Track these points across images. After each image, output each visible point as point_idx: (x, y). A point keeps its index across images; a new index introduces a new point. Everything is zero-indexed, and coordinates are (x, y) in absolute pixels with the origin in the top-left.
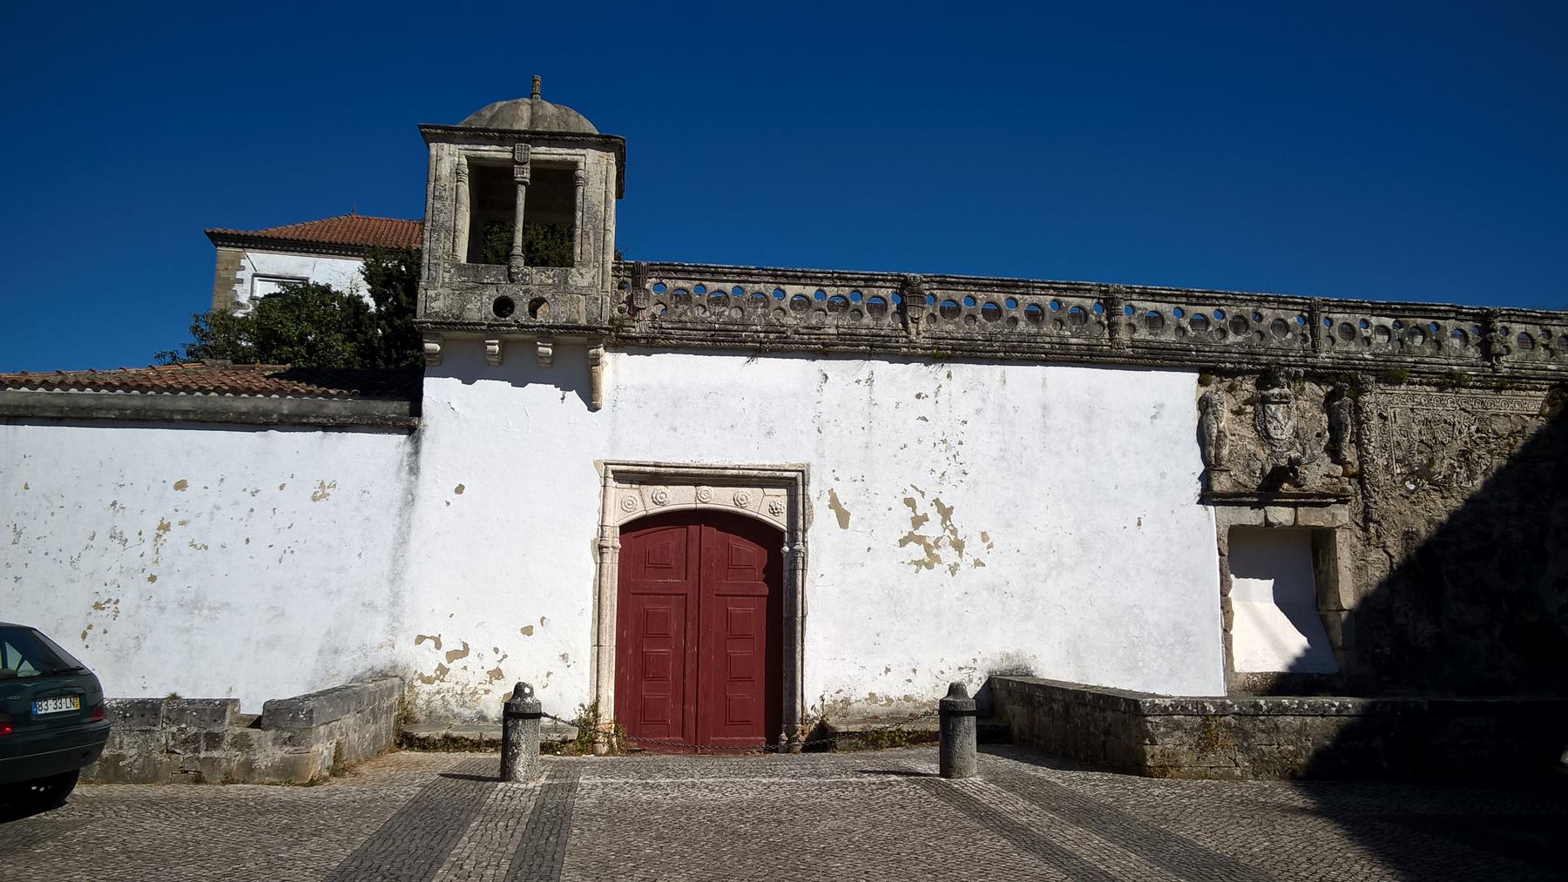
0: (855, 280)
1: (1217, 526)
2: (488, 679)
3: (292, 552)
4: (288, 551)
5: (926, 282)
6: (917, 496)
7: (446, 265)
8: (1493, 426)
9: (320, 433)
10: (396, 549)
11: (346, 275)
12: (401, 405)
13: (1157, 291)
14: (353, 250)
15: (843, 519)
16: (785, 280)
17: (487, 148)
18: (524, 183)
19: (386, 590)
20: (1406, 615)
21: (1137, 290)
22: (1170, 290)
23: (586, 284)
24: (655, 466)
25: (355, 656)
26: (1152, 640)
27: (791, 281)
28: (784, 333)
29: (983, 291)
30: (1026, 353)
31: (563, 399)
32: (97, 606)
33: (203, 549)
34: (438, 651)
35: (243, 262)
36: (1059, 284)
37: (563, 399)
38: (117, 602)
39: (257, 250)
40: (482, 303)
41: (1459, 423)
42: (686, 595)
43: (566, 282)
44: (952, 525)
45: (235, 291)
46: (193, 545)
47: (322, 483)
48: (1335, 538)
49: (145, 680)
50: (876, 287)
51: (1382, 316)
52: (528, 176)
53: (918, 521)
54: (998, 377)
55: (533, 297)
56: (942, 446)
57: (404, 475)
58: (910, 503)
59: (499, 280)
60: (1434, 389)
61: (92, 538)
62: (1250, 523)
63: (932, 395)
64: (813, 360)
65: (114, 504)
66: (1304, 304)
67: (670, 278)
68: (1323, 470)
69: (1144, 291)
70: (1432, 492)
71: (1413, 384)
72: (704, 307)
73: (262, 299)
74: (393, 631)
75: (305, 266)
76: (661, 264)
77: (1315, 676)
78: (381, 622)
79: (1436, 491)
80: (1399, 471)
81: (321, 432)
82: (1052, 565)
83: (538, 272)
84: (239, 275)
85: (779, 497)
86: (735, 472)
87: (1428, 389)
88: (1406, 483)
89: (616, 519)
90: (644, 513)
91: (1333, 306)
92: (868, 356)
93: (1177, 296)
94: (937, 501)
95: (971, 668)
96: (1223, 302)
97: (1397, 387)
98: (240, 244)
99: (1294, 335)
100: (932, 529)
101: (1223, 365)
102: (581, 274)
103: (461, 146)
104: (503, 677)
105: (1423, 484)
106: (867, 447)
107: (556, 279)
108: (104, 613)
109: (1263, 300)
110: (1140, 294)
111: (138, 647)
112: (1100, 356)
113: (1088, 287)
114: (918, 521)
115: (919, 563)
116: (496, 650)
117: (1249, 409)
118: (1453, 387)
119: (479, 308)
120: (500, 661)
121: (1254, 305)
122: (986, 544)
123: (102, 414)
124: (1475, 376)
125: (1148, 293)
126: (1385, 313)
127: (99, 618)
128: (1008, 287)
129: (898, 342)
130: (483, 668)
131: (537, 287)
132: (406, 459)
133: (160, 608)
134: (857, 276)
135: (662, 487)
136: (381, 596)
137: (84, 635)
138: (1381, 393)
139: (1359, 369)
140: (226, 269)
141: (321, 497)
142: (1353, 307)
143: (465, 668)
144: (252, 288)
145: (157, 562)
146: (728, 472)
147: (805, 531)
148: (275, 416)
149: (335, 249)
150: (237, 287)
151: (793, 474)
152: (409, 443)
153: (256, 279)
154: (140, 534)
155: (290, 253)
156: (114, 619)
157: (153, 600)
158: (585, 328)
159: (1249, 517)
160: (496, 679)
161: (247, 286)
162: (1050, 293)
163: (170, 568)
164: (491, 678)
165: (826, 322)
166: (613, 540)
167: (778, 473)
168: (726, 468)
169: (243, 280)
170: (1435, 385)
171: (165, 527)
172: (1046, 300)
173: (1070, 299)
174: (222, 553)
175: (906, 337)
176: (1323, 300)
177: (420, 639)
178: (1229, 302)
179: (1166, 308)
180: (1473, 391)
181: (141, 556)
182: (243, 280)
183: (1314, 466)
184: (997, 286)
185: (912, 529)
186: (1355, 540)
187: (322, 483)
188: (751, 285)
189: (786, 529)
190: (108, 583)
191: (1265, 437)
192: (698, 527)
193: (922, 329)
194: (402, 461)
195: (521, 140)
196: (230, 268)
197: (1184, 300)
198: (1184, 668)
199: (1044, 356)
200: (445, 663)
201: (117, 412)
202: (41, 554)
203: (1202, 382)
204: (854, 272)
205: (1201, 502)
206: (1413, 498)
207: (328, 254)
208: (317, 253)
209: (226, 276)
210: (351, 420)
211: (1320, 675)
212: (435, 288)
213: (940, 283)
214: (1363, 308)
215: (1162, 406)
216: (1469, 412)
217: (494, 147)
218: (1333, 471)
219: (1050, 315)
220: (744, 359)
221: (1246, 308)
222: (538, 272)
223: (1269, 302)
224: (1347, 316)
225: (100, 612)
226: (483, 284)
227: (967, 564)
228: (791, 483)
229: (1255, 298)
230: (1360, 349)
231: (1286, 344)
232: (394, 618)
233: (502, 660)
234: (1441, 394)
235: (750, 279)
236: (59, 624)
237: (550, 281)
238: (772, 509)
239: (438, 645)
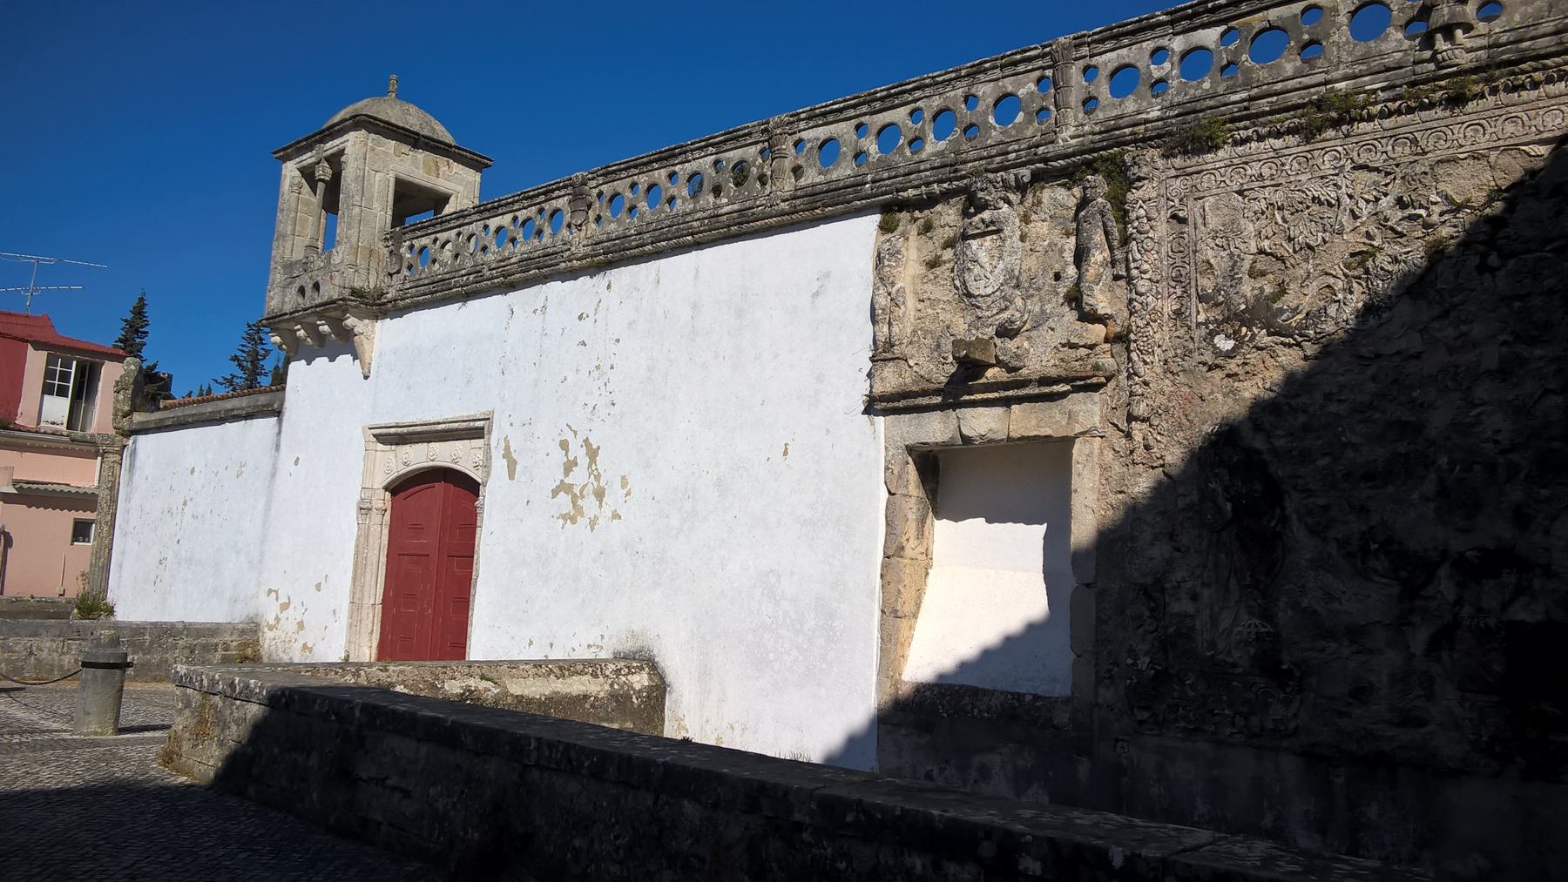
1: (886, 448)
5: (593, 179)
6: (569, 436)
8: (1441, 187)
13: (827, 109)
18: (322, 180)
20: (1194, 597)
21: (802, 116)
22: (845, 101)
26: (789, 622)
27: (492, 214)
28: (480, 272)
29: (643, 173)
30: (671, 239)
36: (717, 137)
41: (1350, 197)
44: (596, 469)
48: (1071, 455)
50: (554, 199)
51: (1195, 29)
53: (569, 466)
54: (652, 278)
56: (596, 374)
57: (273, 452)
58: (564, 445)
60: (1291, 140)
62: (933, 440)
63: (591, 315)
66: (1043, 56)
67: (417, 238)
68: (1059, 337)
69: (812, 113)
70: (1280, 350)
71: (1244, 141)
77: (1029, 698)
79: (1289, 346)
80: (1202, 318)
82: (685, 515)
87: (1278, 143)
88: (1216, 341)
89: (381, 479)
91: (1094, 42)
93: (854, 107)
94: (586, 441)
95: (598, 647)
96: (918, 94)
97: (1209, 157)
99: (1027, 114)
100: (579, 477)
101: (905, 194)
105: (1254, 336)
109: (976, 72)
110: (809, 118)
112: (748, 223)
113: (746, 131)
114: (569, 466)
115: (564, 517)
117: (948, 254)
118: (1336, 124)
121: (965, 83)
122: (625, 491)
124: (1383, 89)
125: (817, 116)
126: (1197, 21)
128: (666, 159)
129: (562, 257)
138: (1177, 177)
139: (1127, 143)
142: (1133, 33)
146: (440, 427)
159: (935, 428)
162: (709, 152)
165: (516, 251)
166: (383, 500)
167: (472, 424)
168: (439, 423)
170: (1291, 131)
172: (705, 163)
173: (731, 154)
176: (1075, 39)
177: (270, 591)
178: (928, 92)
179: (843, 130)
180: (1387, 123)
183: (1043, 330)
184: (656, 161)
185: (562, 477)
186: (1109, 455)
188: (467, 227)
191: (964, 294)
193: (579, 241)
197: (865, 109)
198: (824, 666)
199: (689, 238)
203: (886, 228)
204: (536, 187)
205: (867, 411)
206: (1232, 366)
211: (1036, 697)
213: (604, 175)
214: (1152, 27)
215: (828, 275)
216: (1377, 170)
218: (1081, 336)
219: (709, 182)
221: (952, 93)
223: (985, 71)
224: (1125, 51)
227: (605, 517)
229: (963, 72)
230: (1145, 104)
231: (1014, 132)
234: (1308, 147)
235: (466, 221)
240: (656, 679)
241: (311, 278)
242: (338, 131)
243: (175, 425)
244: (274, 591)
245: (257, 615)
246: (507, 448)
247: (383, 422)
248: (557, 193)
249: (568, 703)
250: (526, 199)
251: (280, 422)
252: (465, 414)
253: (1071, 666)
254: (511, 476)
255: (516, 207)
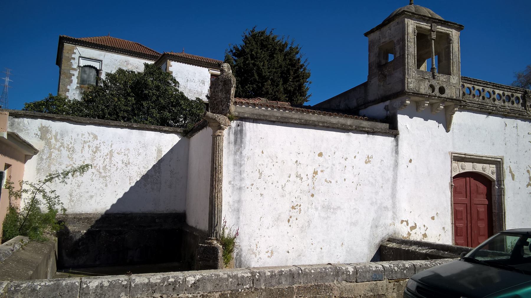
0: (513, 90)
2: (423, 238)
3: (360, 185)
4: (359, 184)
7: (413, 69)
9: (366, 135)
10: (393, 185)
11: (117, 61)
12: (386, 125)
14: (120, 51)
15: (513, 176)
16: (495, 88)
17: (423, 23)
18: (434, 40)
19: (391, 201)
23: (455, 83)
24: (464, 155)
25: (383, 229)
27: (497, 88)
31: (438, 127)
32: (293, 208)
33: (330, 183)
34: (408, 226)
35: (75, 51)
37: (438, 127)
38: (300, 206)
39: (81, 46)
40: (425, 86)
42: (466, 204)
43: (449, 81)
45: (72, 62)
46: (326, 181)
47: (368, 156)
49: (312, 240)
52: (435, 37)
55: (440, 86)
57: (394, 154)
59: (430, 77)
61: (289, 177)
64: (503, 118)
65: (297, 162)
67: (466, 83)
72: (490, 97)
73: (83, 67)
74: (394, 218)
75: (100, 55)
76: (464, 77)
78: (390, 214)
81: (367, 135)
83: (441, 76)
84: (73, 56)
85: (493, 167)
86: (485, 158)
90: (459, 173)
92: (516, 118)
98: (74, 43)
102: (454, 78)
103: (415, 21)
104: (427, 237)
106: (517, 151)
107: (446, 79)
108: (295, 211)
111: (309, 226)
116: (424, 226)
119: (424, 89)
120: (426, 230)
123: (293, 121)
127: (294, 213)
130: (421, 233)
131: (441, 82)
132: (394, 147)
133: (316, 208)
134: (514, 88)
135: (463, 163)
136: (388, 203)
137: (289, 221)
140: (68, 53)
141: (368, 162)
143: (416, 233)
144: (79, 62)
145: (314, 188)
147: (503, 181)
148: (354, 127)
149: (113, 50)
150: (72, 61)
151: (499, 160)
152: (395, 141)
153: (80, 58)
154: (307, 175)
155: (94, 49)
156: (300, 213)
157: (313, 205)
158: (455, 100)
160: (425, 237)
161: (77, 61)
163: (319, 191)
164: (423, 237)
167: (496, 159)
169: (75, 58)
171: (316, 173)
174: (337, 184)
175: (526, 112)
177: (402, 221)
181: (308, 185)
182: (75, 58)
187: (368, 156)
188: (487, 88)
189: (496, 180)
190: (296, 198)
192: (469, 178)
194: (393, 148)
195: (435, 22)
196: (69, 52)
200: (410, 231)
201: (298, 120)
202: (270, 183)
207: (103, 50)
208: (106, 50)
209: (68, 56)
210: (379, 130)
212: (411, 79)
217: (425, 24)
220: (485, 116)
222: (441, 76)
225: (294, 210)
226: (425, 78)
228: (498, 163)
232: (394, 213)
233: (426, 230)
236: (279, 216)
237: (445, 80)
238: (492, 172)
239: (408, 224)
240: (520, 235)
241: (438, 83)
242: (450, 25)
243: (301, 124)
244: (406, 221)
245: (395, 233)
246: (510, 170)
247: (459, 152)
248: (518, 92)
249: (216, 257)
250: (509, 89)
251: (397, 141)
252: (493, 155)
253: (86, 212)
254: (513, 179)
255: (506, 90)
